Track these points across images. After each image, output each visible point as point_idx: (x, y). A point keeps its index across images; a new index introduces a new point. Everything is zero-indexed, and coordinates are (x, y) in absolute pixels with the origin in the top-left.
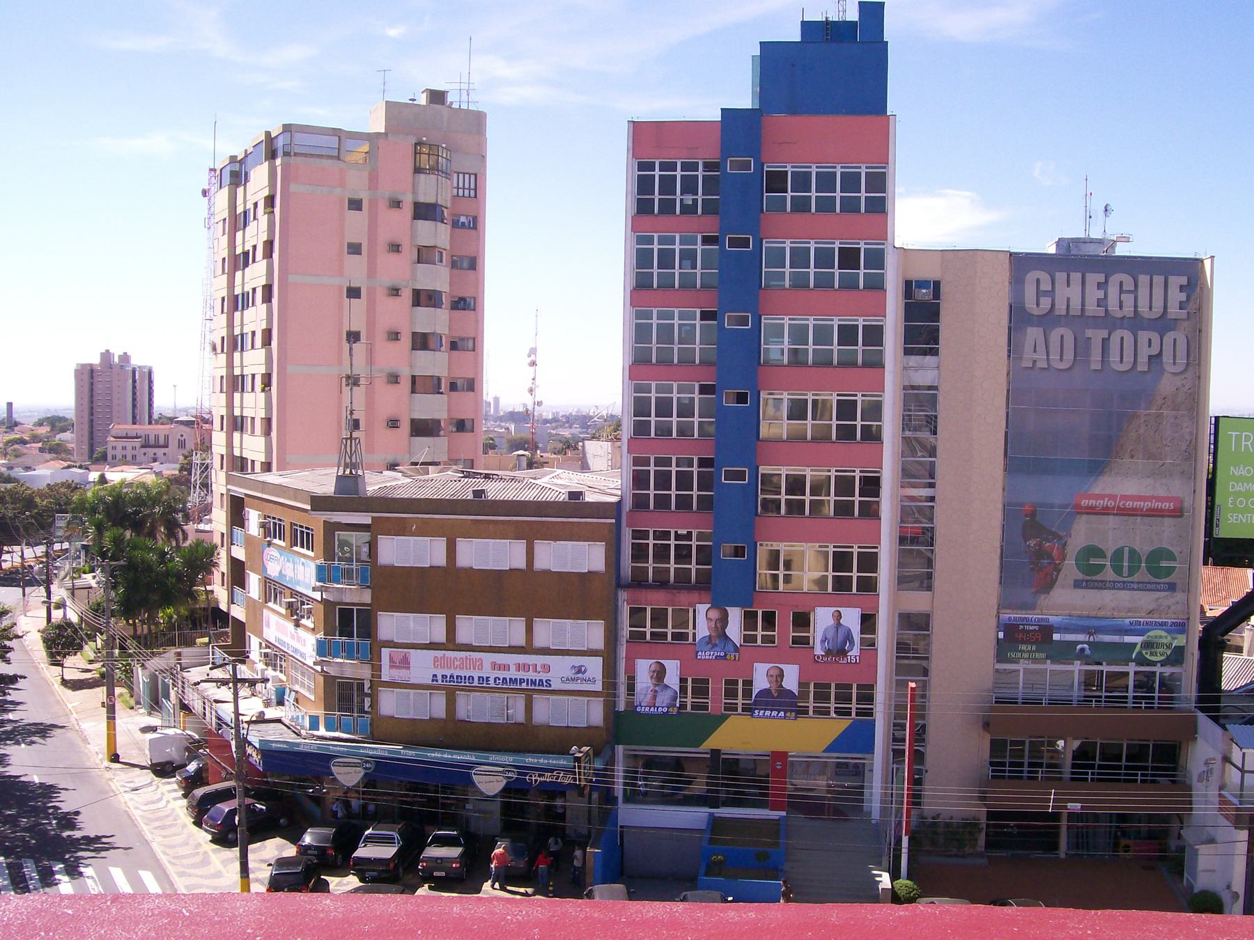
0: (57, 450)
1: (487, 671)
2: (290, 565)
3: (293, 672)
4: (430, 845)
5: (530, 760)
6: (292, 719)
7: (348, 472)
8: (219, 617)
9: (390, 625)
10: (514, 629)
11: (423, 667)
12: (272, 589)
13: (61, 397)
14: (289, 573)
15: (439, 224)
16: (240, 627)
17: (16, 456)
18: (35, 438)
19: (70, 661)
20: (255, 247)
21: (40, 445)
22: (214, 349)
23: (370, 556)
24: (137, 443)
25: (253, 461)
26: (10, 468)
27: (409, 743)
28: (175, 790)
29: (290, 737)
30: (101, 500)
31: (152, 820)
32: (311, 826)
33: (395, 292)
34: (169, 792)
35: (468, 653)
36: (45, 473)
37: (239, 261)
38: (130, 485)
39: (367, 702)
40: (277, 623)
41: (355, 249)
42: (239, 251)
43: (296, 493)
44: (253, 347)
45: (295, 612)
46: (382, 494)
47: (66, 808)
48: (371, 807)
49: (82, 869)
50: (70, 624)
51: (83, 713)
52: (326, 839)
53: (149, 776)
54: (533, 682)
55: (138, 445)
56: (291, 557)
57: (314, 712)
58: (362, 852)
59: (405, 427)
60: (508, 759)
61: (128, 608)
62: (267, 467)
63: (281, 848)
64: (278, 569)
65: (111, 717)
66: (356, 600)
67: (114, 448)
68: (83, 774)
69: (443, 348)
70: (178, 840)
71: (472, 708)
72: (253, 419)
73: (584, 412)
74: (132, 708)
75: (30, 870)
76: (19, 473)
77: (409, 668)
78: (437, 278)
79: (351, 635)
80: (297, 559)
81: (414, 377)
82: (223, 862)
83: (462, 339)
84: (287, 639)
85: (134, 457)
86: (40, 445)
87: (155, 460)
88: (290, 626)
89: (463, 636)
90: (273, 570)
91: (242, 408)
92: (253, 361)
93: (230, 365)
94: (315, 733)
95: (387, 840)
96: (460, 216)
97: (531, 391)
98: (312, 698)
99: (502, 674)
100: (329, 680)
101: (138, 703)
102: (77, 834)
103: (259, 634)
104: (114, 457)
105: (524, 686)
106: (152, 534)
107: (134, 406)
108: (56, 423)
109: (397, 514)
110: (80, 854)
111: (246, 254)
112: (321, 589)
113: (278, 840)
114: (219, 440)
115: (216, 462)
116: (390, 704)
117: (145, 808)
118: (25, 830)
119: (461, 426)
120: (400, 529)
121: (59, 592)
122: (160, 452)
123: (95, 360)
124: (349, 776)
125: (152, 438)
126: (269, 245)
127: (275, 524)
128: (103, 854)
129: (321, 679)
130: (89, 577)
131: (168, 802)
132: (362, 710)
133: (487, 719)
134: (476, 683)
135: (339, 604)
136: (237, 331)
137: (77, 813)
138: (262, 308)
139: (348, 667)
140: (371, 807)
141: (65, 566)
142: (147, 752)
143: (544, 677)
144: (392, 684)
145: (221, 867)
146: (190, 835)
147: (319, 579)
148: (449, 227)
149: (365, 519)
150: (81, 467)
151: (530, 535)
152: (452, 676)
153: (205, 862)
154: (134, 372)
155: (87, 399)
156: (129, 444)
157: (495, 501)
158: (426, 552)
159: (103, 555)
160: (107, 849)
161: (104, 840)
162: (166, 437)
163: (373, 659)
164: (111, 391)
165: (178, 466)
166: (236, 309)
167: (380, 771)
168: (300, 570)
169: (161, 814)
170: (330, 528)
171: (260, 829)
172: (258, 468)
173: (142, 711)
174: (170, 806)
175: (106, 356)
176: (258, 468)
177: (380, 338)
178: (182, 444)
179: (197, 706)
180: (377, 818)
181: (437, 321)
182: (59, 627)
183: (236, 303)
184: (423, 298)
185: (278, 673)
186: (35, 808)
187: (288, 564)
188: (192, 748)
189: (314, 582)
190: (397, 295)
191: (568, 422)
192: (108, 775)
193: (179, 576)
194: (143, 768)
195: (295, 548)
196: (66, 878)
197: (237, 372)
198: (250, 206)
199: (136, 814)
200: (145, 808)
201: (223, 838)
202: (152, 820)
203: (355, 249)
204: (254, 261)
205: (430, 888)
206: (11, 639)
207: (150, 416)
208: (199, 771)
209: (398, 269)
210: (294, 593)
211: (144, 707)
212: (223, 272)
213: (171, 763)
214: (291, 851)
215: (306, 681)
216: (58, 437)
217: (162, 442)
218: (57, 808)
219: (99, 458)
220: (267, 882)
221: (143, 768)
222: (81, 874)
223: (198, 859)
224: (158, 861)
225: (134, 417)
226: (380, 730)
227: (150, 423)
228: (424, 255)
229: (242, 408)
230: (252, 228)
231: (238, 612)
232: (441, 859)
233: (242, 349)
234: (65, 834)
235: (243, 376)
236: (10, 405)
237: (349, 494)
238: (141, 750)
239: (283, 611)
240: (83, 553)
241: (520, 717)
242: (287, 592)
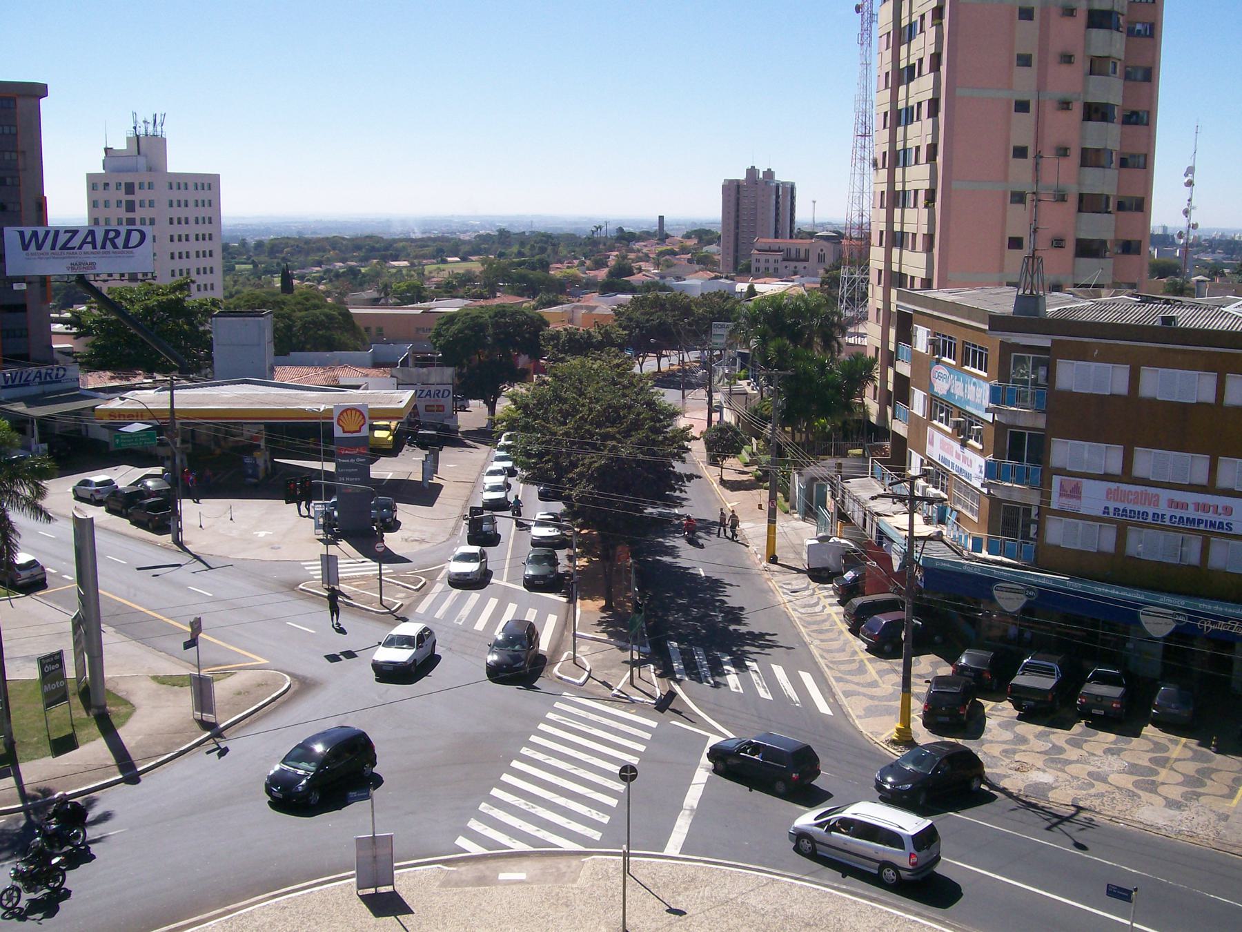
0: (705, 262)
1: (1163, 508)
2: (961, 384)
3: (955, 492)
4: (1089, 681)
5: (1204, 606)
6: (954, 539)
7: (1028, 292)
8: (881, 431)
9: (1062, 452)
10: (1196, 467)
11: (1094, 497)
12: (938, 406)
13: (707, 209)
14: (958, 391)
15: (1115, 32)
16: (900, 444)
17: (668, 267)
18: (684, 250)
19: (730, 462)
20: (921, 61)
21: (689, 256)
22: (875, 164)
23: (1047, 379)
24: (779, 256)
25: (913, 278)
26: (662, 277)
27: (1076, 575)
28: (831, 596)
29: (950, 556)
30: (762, 311)
31: (810, 624)
32: (969, 646)
33: (1065, 105)
34: (825, 597)
35: (1144, 488)
36: (696, 283)
37: (902, 75)
38: (790, 297)
39: (1033, 529)
40: (942, 441)
41: (1025, 61)
42: (903, 64)
43: (971, 312)
44: (916, 163)
45: (963, 431)
46: (1062, 316)
47: (732, 602)
48: (1027, 635)
49: (748, 663)
50: (729, 427)
51: (749, 512)
52: (982, 662)
53: (803, 581)
54: (1212, 524)
55: (780, 258)
56: (962, 376)
57: (976, 534)
58: (1020, 680)
59: (1070, 247)
60: (1180, 602)
61: (789, 417)
62: (927, 283)
63: (935, 665)
64: (946, 387)
65: (772, 520)
66: (1029, 424)
67: (757, 261)
68: (744, 572)
69: (1113, 165)
70: (835, 645)
71: (1140, 545)
72: (914, 235)
73: (1229, 236)
74: (787, 512)
75: (700, 657)
76: (670, 281)
77: (1079, 498)
78: (1110, 91)
79: (1020, 459)
80: (968, 378)
81: (1081, 195)
82: (878, 672)
83: (1133, 156)
84: (952, 459)
85: (776, 270)
86: (689, 256)
87: (795, 274)
88: (956, 446)
89: (1224, 481)
90: (941, 387)
91: (902, 223)
92: (917, 177)
93: (891, 180)
94: (979, 555)
95: (1047, 672)
96: (1135, 23)
97: (1186, 212)
98: (976, 519)
99: (1178, 513)
100: (994, 502)
101: (793, 507)
102: (743, 629)
103: (922, 451)
104: (758, 269)
105: (1202, 527)
106: (809, 345)
107: (777, 220)
108: (703, 235)
109: (1079, 338)
110: (747, 648)
111: (911, 68)
112: (993, 411)
113: (932, 657)
114: (877, 256)
115: (873, 277)
116: (1056, 533)
117: (803, 611)
118: (694, 619)
119: (1129, 248)
120: (1081, 354)
121: (718, 397)
122: (800, 265)
123: (742, 176)
124: (1011, 602)
125: (793, 252)
126: (936, 59)
127: (945, 342)
128: (767, 651)
129: (987, 501)
130: (744, 383)
131: (824, 607)
132: (1026, 536)
133: (1158, 558)
134: (1150, 520)
135: (1012, 427)
136: (900, 146)
137: (742, 609)
138: (927, 123)
139: (1014, 490)
140: (1027, 635)
141: (722, 370)
142: (805, 557)
143: (1225, 519)
144: (1061, 513)
145: (876, 677)
146: (846, 642)
147: (992, 400)
148: (1124, 35)
149: (1044, 341)
150: (727, 278)
151: (1222, 368)
152: (1124, 510)
153: (862, 670)
154: (777, 187)
155: (733, 214)
156: (772, 257)
157: (1189, 330)
158: (1109, 379)
159: (767, 364)
160: (771, 647)
161: (768, 637)
162: (807, 251)
163: (1044, 487)
164: (757, 203)
165: (819, 280)
166: (899, 124)
167: (1044, 599)
168: (974, 392)
169: (819, 618)
170: (1006, 348)
171: (922, 645)
172: (917, 285)
173: (796, 516)
174: (826, 611)
175: (752, 172)
176: (917, 285)
177: (1048, 154)
178: (821, 259)
179: (857, 517)
180: (1039, 645)
181: (1109, 136)
182: (721, 430)
183: (899, 118)
184: (1096, 112)
185: (938, 491)
186: (703, 600)
187: (958, 383)
188: (850, 559)
189: (986, 403)
190: (1068, 109)
191: (1210, 246)
192: (767, 575)
193: (838, 388)
194: (800, 571)
195: (966, 368)
196: (733, 670)
197: (898, 187)
198: (916, 17)
199: (795, 615)
200: (803, 611)
201: (883, 646)
202: (810, 624)
203: (1025, 61)
204: (920, 74)
205: (1087, 724)
206: (689, 441)
207: (791, 231)
208: (855, 579)
209: (1067, 81)
210: (963, 412)
211: (798, 512)
212: (886, 87)
213: (826, 569)
214: (946, 670)
215: (969, 501)
216: (705, 249)
217: (802, 255)
218: (723, 602)
219: (744, 271)
220: (924, 698)
221: (800, 571)
222: (747, 667)
223: (855, 666)
224: (816, 663)
225: (776, 232)
226: (1044, 558)
227: (791, 237)
228: (1097, 66)
229: (902, 223)
230: (917, 43)
231: (899, 427)
232: (1102, 697)
233: (905, 165)
234: (732, 628)
235: (904, 191)
236: (661, 218)
237: (1028, 315)
238: (798, 554)
239: (949, 430)
240: (738, 360)
241: (1194, 558)
242: (955, 411)
